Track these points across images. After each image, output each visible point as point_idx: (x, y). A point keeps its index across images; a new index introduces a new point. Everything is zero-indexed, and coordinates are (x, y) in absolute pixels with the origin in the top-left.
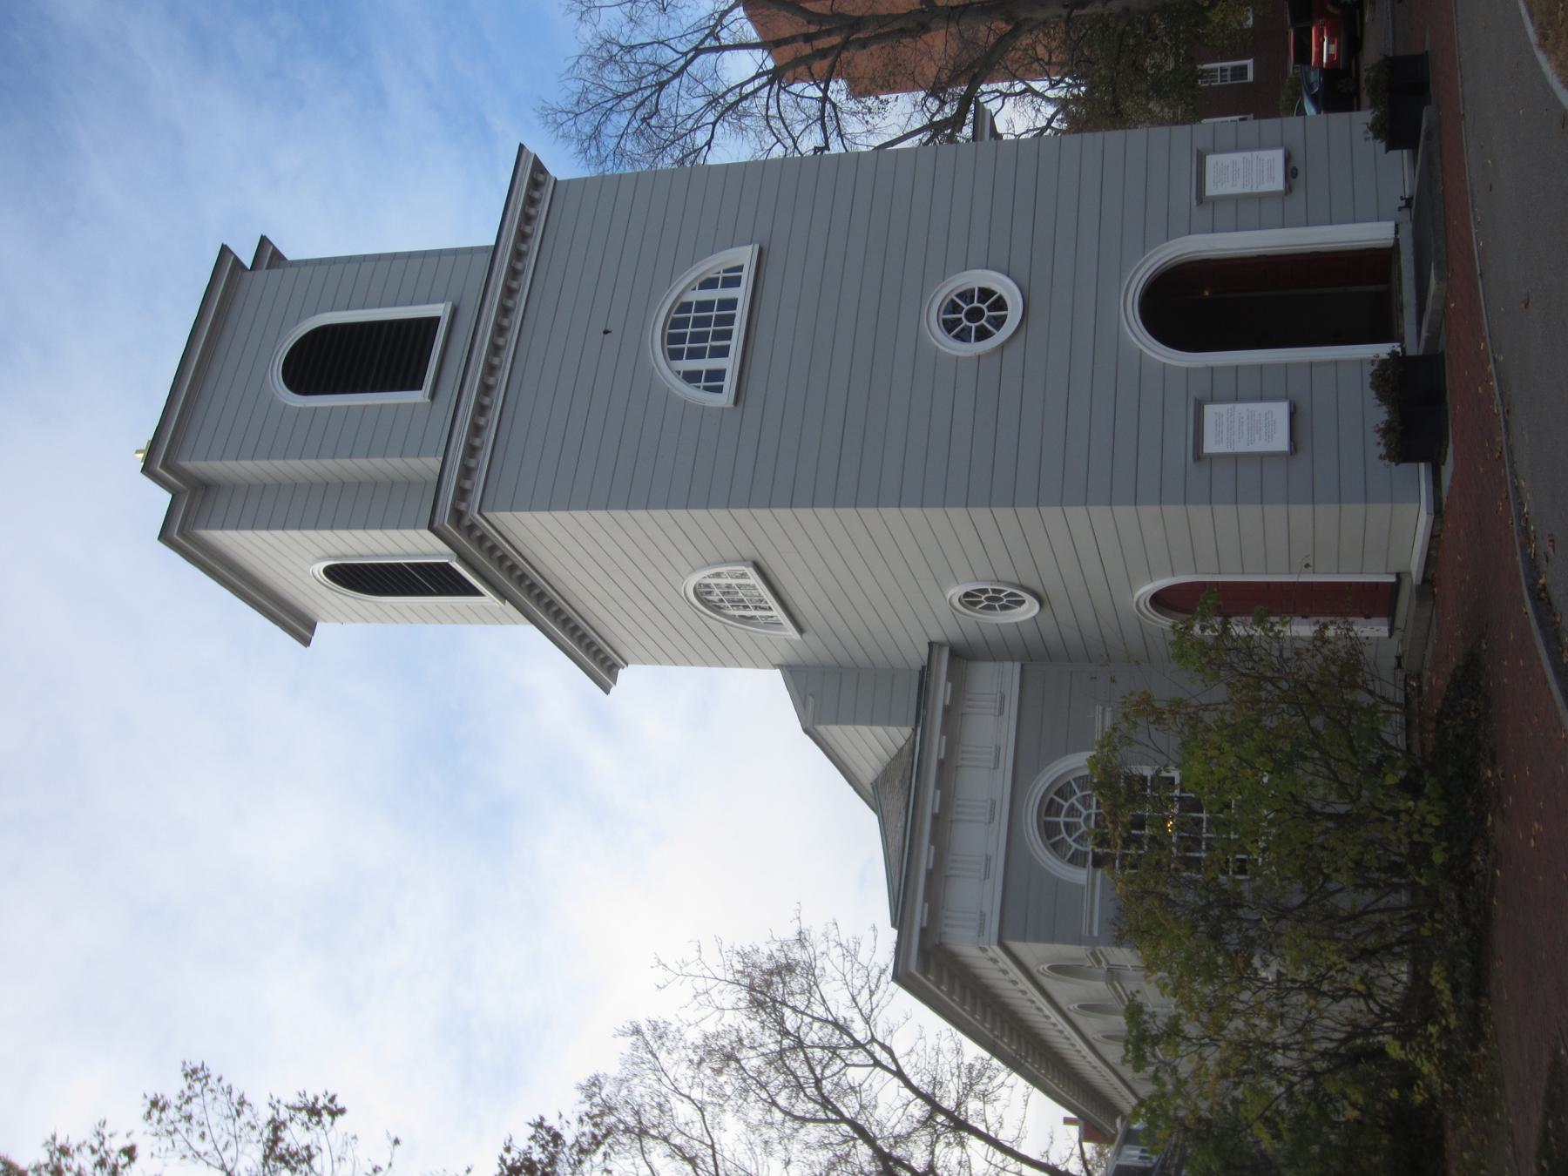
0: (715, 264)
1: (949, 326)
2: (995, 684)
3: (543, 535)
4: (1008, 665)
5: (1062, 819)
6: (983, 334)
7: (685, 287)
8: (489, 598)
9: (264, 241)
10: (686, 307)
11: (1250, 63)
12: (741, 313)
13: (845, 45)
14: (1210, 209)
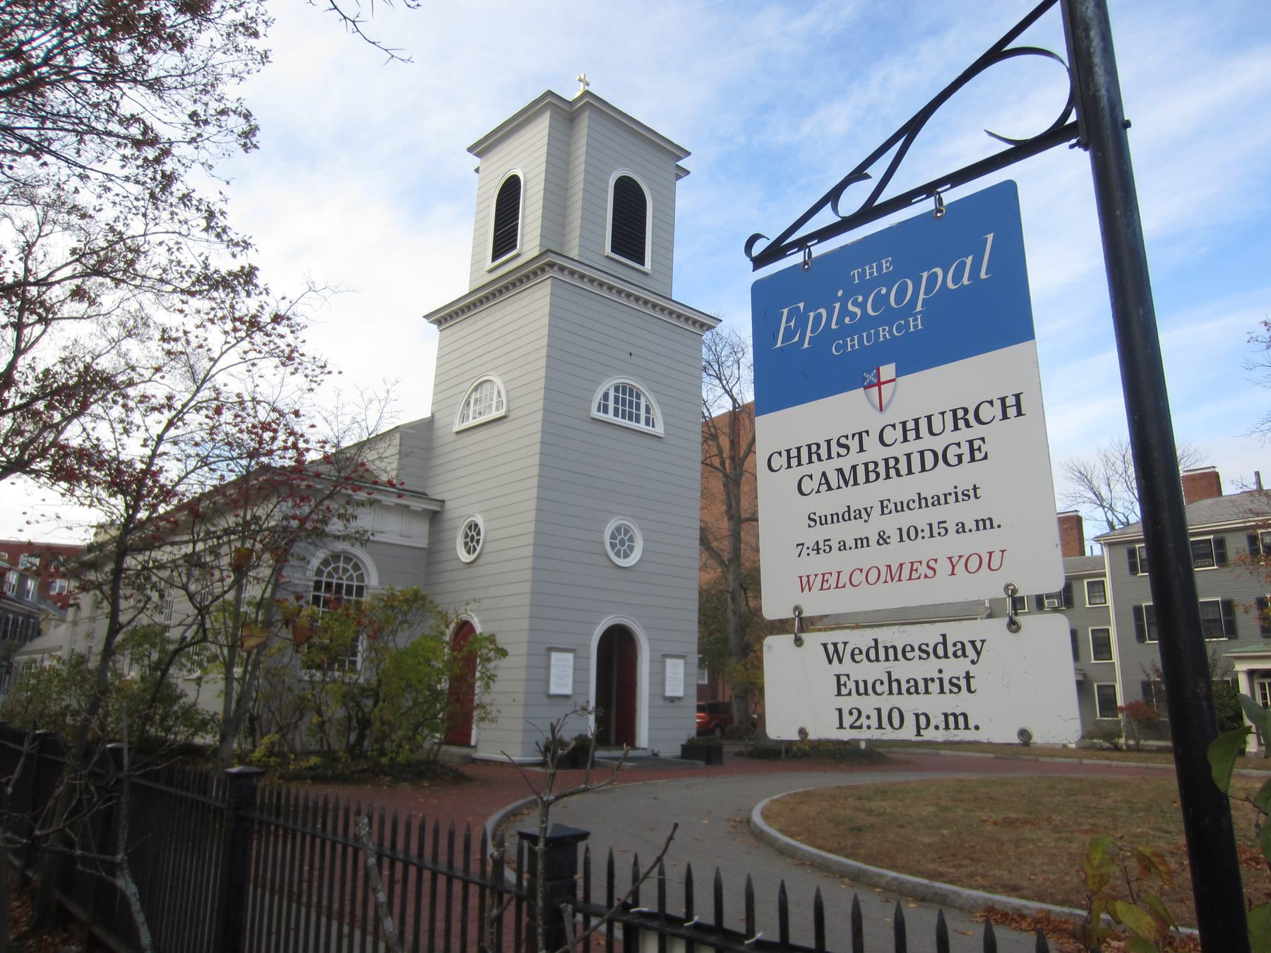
0: (657, 414)
1: (618, 529)
2: (417, 534)
3: (536, 303)
6: (613, 545)
7: (647, 398)
8: (489, 264)
10: (638, 397)
12: (633, 425)
13: (726, 476)
14: (661, 659)
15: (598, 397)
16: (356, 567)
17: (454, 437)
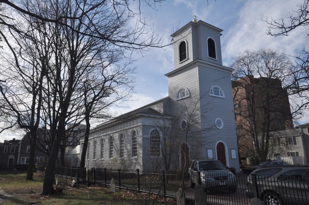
1: (218, 120)
10: (218, 90)
11: (27, 152)
12: (218, 96)
14: (230, 150)
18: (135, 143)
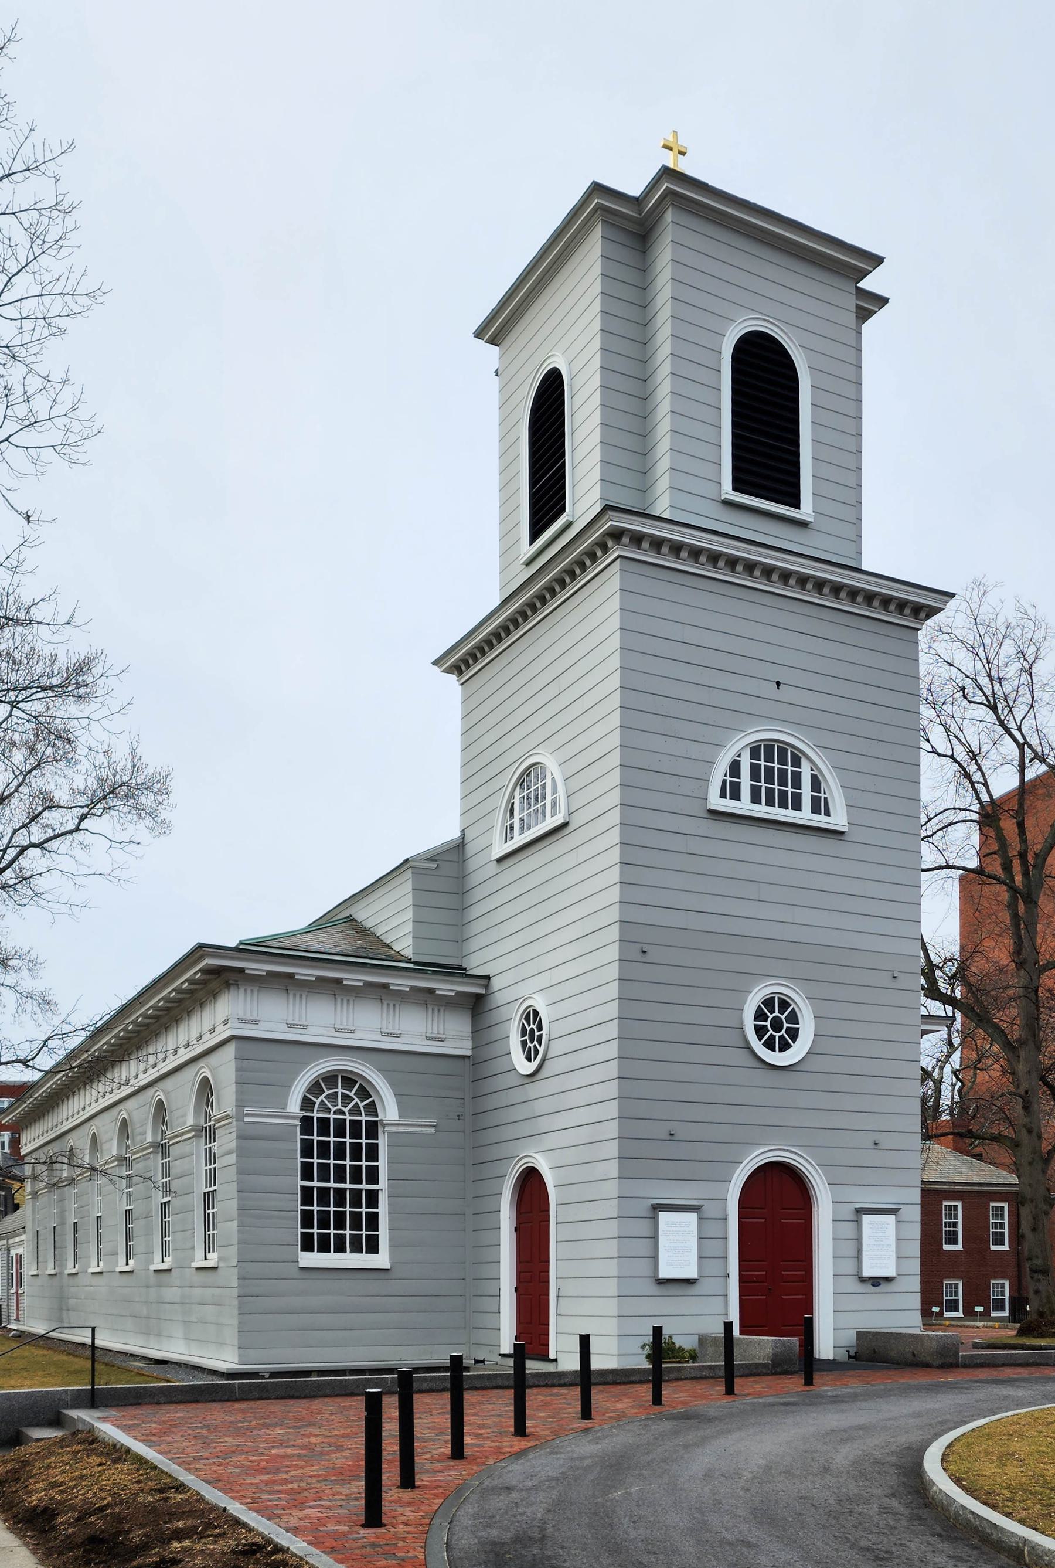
1: (769, 1002)
2: (454, 1036)
3: (598, 613)
4: (469, 1044)
5: (340, 1090)
6: (760, 1031)
7: (816, 760)
8: (527, 550)
9: (883, 301)
10: (797, 763)
11: (959, 1247)
12: (788, 815)
15: (719, 773)
16: (364, 1094)
17: (493, 868)
18: (209, 1167)
